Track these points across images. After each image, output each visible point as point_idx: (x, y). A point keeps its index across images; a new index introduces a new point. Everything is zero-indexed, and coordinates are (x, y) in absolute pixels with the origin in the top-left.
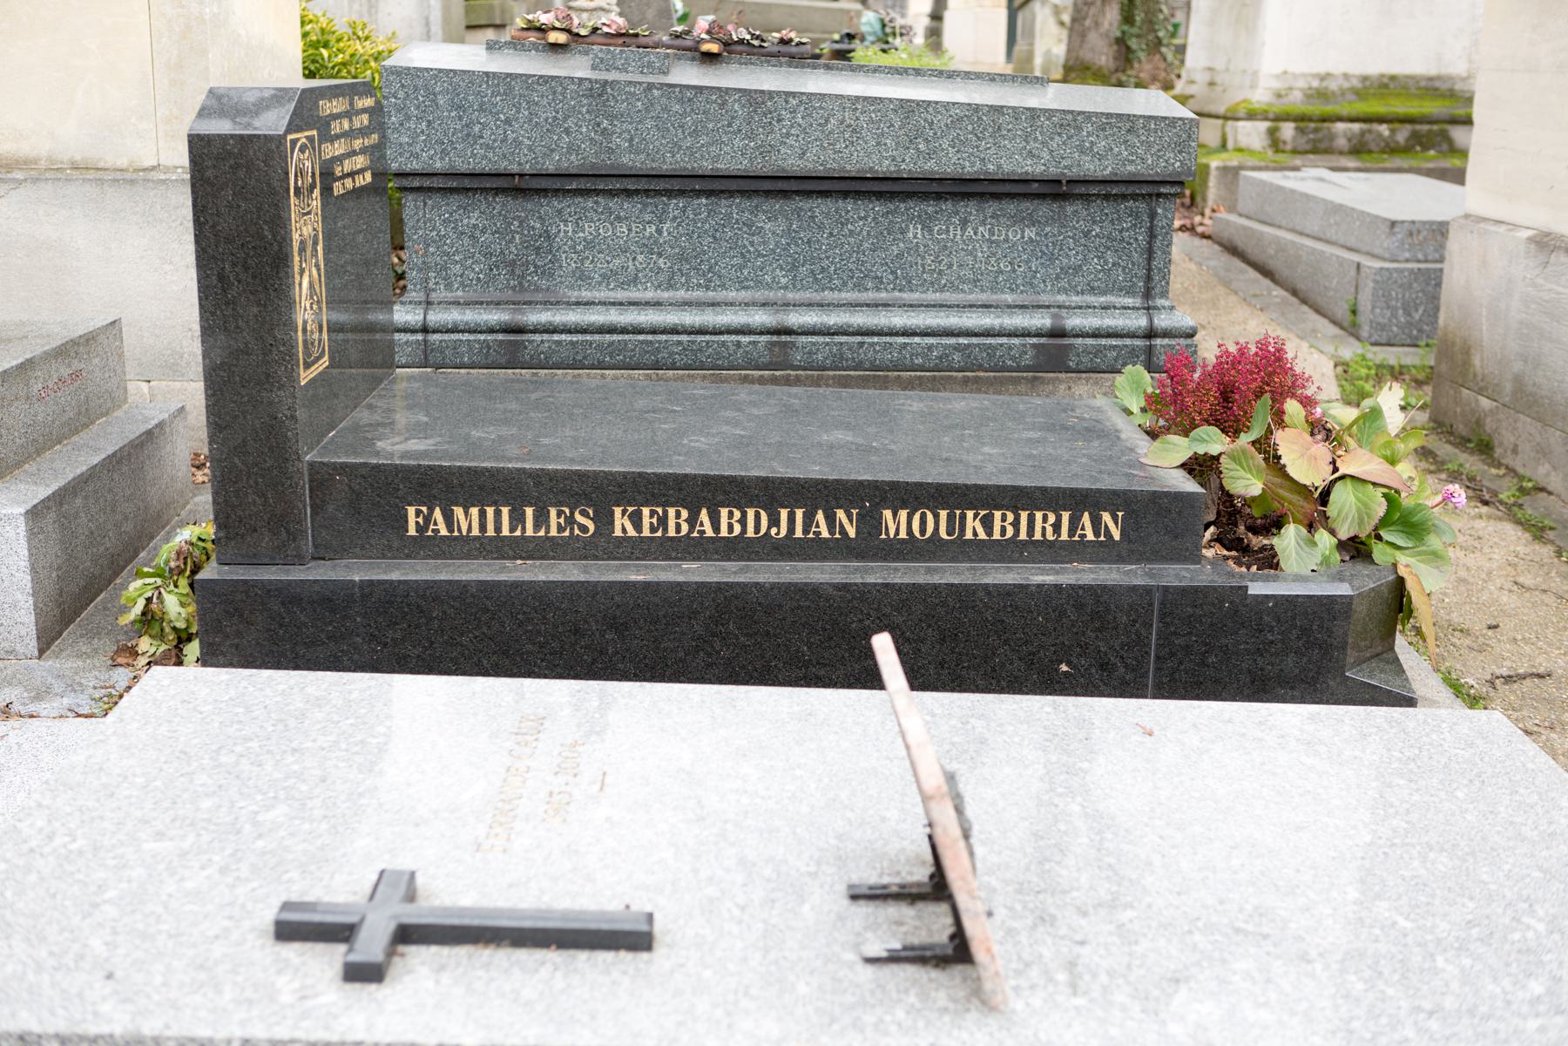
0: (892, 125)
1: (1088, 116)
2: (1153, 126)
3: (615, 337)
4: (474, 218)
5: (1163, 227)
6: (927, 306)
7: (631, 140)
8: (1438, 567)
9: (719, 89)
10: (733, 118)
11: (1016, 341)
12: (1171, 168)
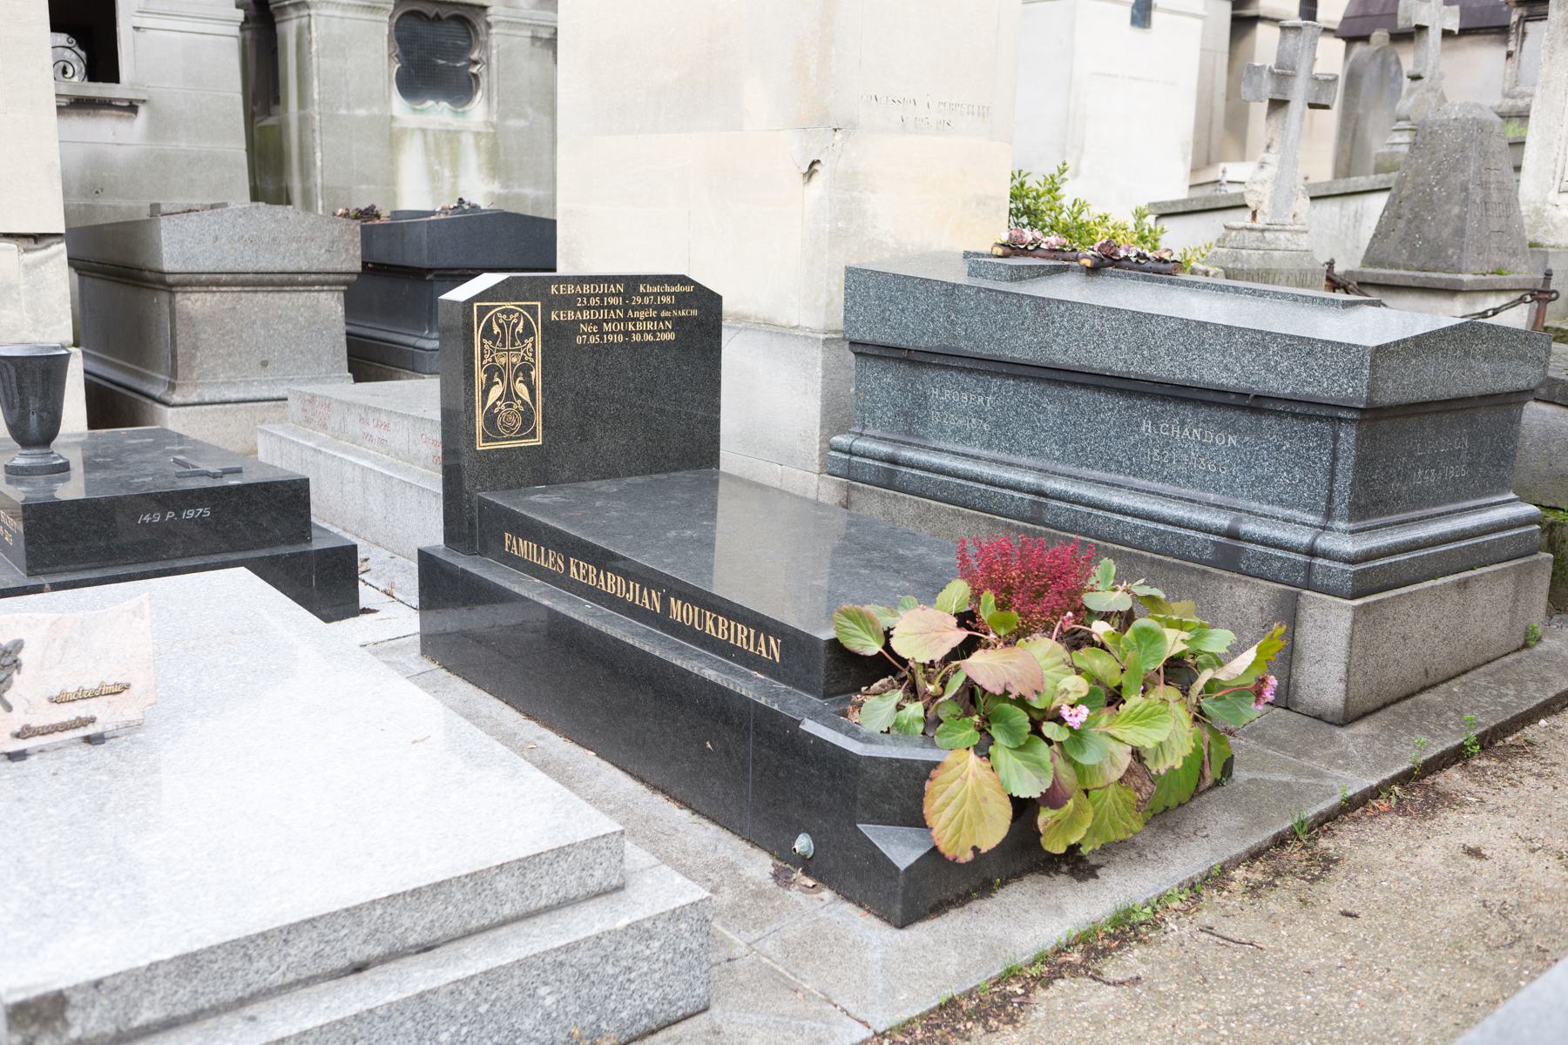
0: (1126, 333)
1: (1275, 336)
2: (1329, 351)
3: (945, 478)
4: (888, 379)
5: (1344, 451)
6: (1148, 492)
7: (966, 330)
8: (1040, 778)
9: (1018, 294)
10: (1025, 318)
11: (1201, 535)
12: (1344, 393)
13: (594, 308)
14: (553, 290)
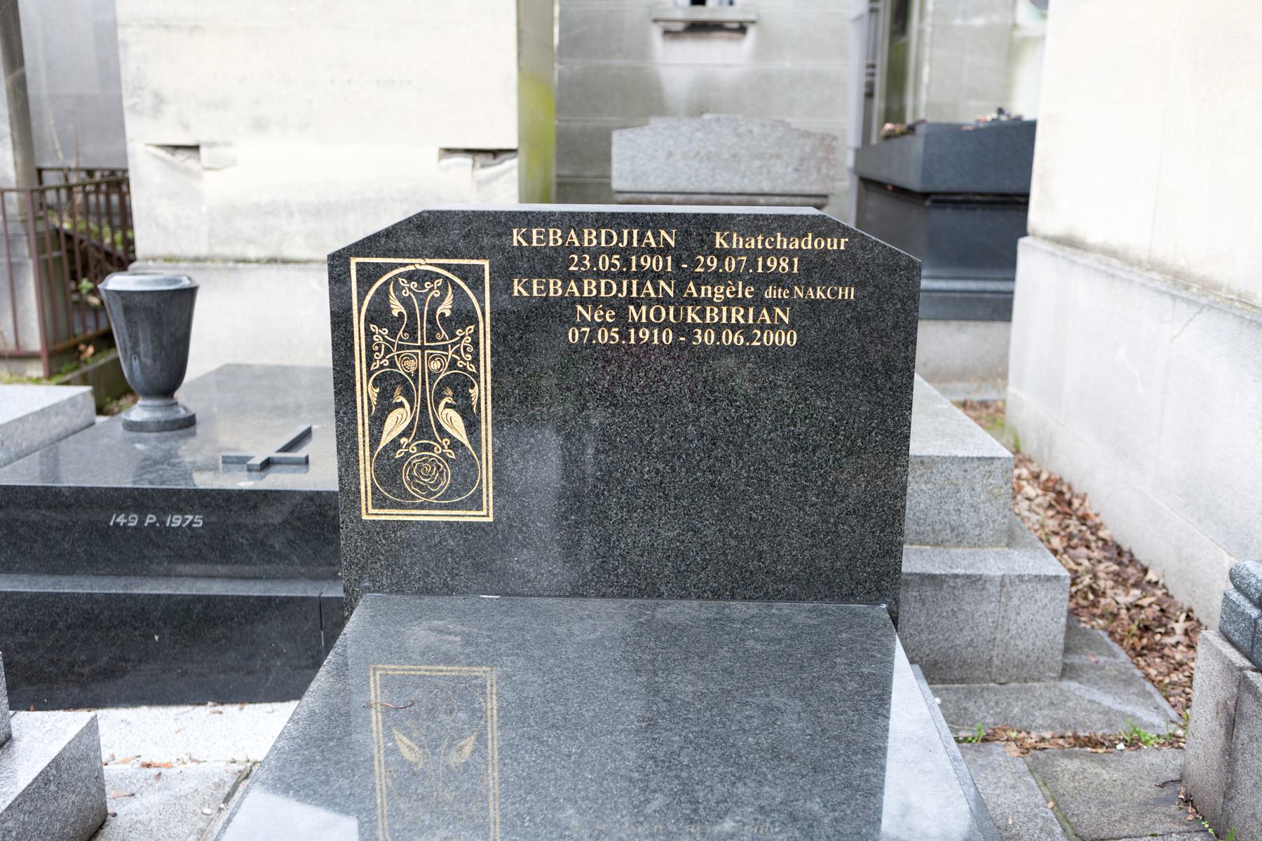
13: (606, 275)
14: (517, 238)
